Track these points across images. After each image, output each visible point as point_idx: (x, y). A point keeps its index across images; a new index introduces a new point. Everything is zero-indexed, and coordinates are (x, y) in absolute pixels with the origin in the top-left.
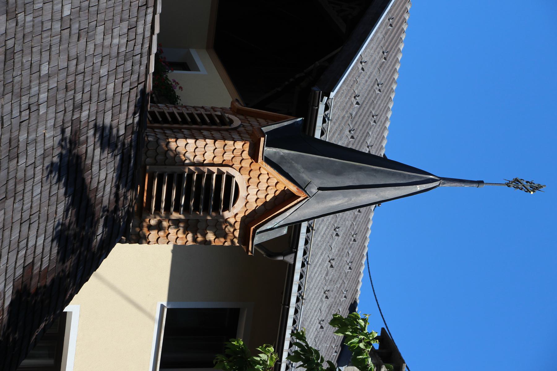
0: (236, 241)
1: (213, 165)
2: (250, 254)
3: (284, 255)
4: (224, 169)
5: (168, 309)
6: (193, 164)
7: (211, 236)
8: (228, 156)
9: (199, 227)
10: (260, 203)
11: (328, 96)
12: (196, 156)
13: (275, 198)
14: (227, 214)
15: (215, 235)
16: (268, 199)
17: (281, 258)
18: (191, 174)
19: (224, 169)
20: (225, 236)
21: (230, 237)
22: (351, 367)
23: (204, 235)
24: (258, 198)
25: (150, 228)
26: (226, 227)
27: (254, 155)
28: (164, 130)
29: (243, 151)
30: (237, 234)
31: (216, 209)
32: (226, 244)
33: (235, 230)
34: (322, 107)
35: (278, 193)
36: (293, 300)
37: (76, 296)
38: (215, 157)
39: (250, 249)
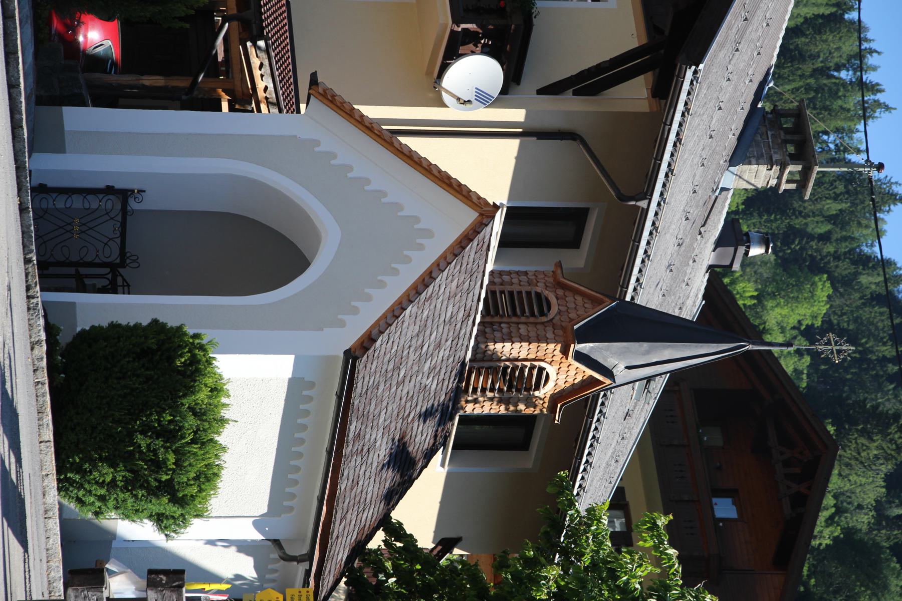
0: (545, 410)
1: (526, 360)
2: (556, 422)
3: (637, 201)
4: (536, 363)
5: (507, 207)
6: (508, 360)
7: (522, 407)
8: (540, 355)
9: (511, 401)
10: (568, 385)
11: (697, 66)
12: (511, 354)
13: (583, 381)
14: (537, 393)
15: (526, 405)
16: (576, 382)
17: (633, 203)
18: (506, 367)
19: (536, 363)
20: (535, 406)
21: (540, 407)
22: (747, 166)
23: (516, 405)
24: (567, 381)
25: (467, 402)
26: (537, 400)
27: (565, 352)
28: (486, 327)
29: (555, 350)
30: (546, 405)
31: (528, 389)
32: (536, 412)
33: (544, 403)
34: (689, 74)
35: (585, 378)
36: (646, 234)
37: (401, 501)
38: (529, 354)
39: (557, 418)
